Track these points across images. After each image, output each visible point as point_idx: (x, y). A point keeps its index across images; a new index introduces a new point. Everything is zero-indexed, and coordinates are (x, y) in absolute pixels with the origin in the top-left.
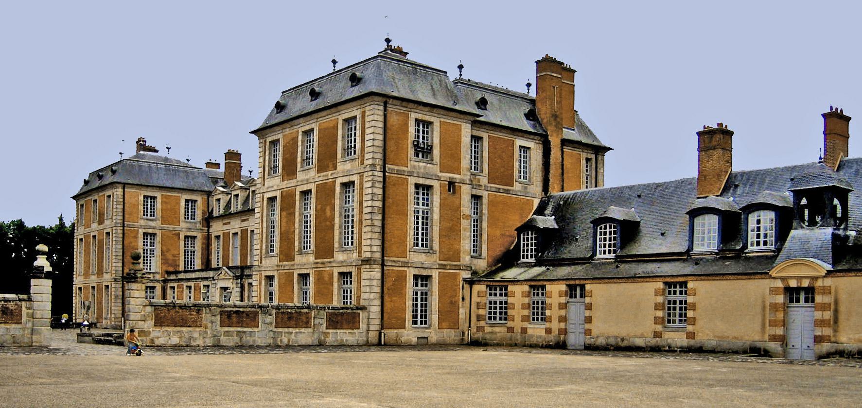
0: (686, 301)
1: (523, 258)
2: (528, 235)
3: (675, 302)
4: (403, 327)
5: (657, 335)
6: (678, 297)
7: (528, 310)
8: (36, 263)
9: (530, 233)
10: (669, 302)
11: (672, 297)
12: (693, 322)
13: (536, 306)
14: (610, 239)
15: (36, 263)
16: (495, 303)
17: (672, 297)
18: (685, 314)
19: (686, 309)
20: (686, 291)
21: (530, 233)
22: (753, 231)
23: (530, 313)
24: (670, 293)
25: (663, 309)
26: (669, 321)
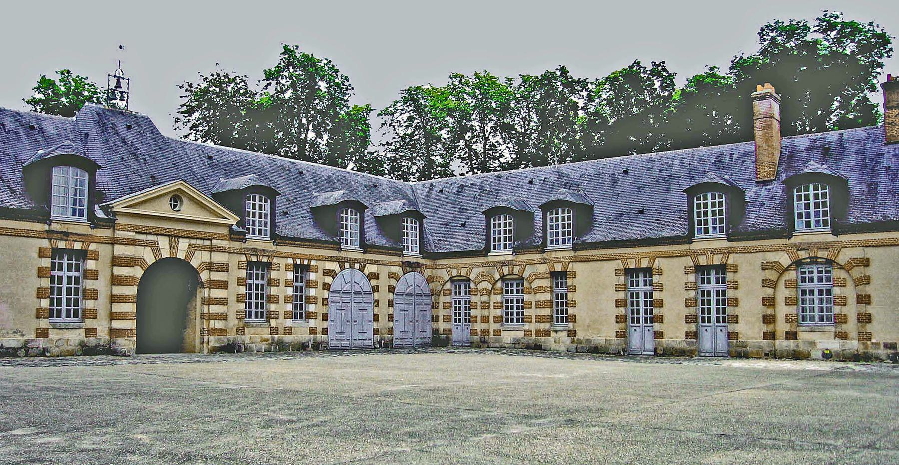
0: (523, 300)
1: (495, 248)
2: (500, 220)
3: (512, 301)
4: (766, 337)
5: (43, 333)
6: (515, 296)
7: (795, 306)
8: (849, 54)
9: (560, 211)
10: (507, 301)
11: (510, 296)
12: (660, 319)
13: (510, 304)
14: (505, 231)
15: (849, 54)
16: (811, 292)
17: (510, 296)
18: (523, 313)
19: (523, 308)
20: (522, 290)
21: (560, 211)
22: (800, 216)
23: (797, 309)
24: (507, 292)
25: (625, 305)
26: (507, 320)
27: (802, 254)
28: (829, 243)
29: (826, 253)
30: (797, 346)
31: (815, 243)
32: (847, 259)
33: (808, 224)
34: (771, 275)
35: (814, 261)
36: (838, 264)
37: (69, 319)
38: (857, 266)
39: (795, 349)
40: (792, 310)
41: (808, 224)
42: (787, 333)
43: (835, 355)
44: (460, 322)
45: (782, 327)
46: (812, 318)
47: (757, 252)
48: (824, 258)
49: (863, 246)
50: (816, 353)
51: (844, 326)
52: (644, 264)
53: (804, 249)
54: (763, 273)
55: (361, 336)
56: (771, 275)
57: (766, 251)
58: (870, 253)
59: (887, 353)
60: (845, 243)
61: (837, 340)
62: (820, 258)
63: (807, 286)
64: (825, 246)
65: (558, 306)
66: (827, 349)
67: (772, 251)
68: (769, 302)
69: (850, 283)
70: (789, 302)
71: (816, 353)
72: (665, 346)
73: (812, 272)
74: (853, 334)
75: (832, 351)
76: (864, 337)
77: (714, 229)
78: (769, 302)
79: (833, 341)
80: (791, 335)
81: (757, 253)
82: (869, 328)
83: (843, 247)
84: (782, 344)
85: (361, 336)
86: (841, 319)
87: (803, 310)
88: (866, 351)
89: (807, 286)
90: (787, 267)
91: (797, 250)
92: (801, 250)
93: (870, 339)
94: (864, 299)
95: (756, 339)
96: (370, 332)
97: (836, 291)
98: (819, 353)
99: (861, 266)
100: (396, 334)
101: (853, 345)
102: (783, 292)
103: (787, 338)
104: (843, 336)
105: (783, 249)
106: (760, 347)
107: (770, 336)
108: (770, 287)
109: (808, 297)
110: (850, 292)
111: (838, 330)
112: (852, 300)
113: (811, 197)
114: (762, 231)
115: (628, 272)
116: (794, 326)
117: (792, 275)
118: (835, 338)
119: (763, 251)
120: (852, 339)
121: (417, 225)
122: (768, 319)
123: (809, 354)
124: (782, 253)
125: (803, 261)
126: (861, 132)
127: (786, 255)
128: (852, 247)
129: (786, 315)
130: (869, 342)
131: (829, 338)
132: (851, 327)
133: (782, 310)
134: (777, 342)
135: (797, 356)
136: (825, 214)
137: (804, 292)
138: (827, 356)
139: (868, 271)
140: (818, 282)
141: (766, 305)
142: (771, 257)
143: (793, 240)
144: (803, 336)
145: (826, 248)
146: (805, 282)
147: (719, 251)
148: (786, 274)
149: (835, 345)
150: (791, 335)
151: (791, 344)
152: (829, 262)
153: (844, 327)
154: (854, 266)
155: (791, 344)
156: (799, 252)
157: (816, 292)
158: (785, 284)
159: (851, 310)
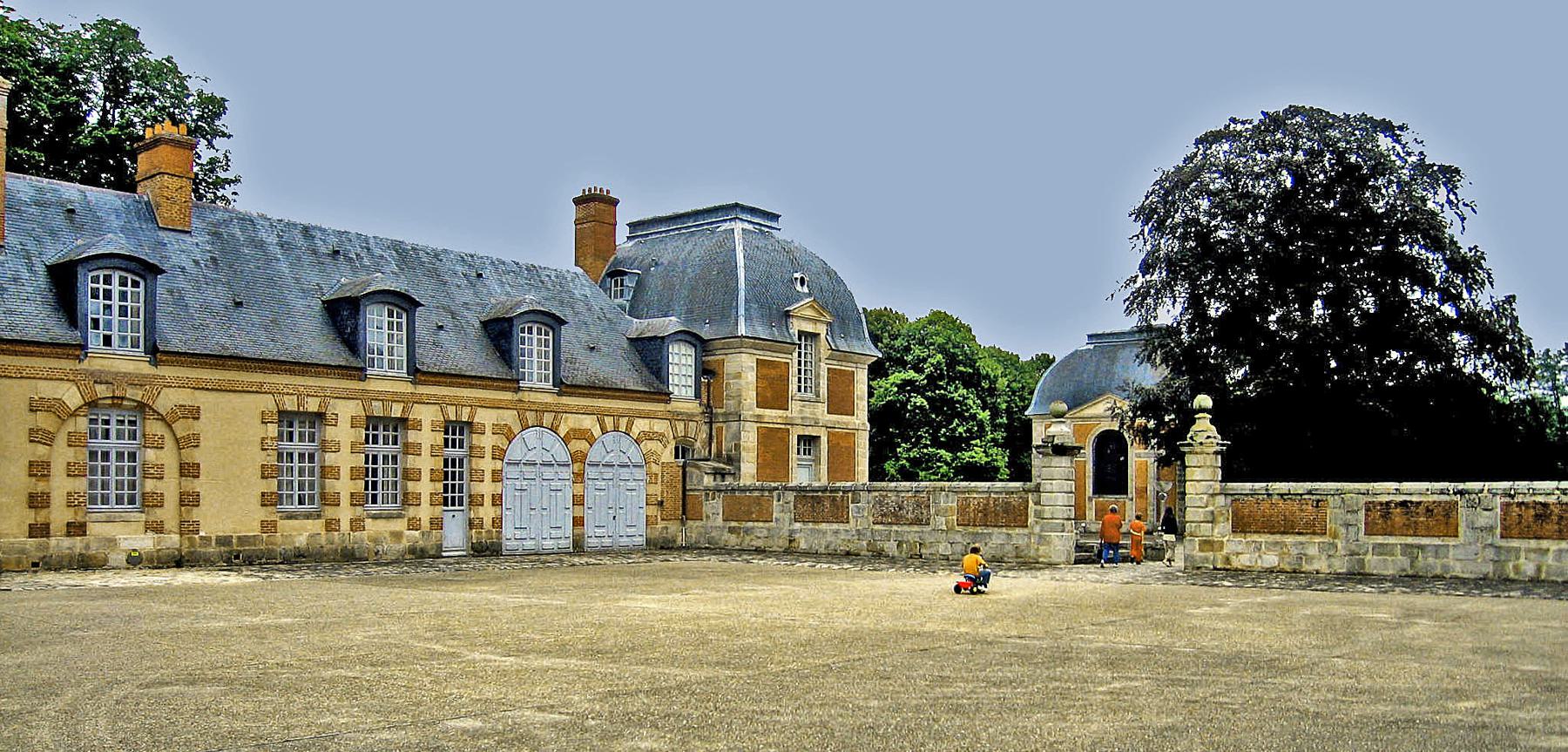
23: (142, 485)
27: (102, 390)
28: (145, 376)
29: (141, 393)
30: (87, 547)
31: (125, 373)
32: (170, 405)
33: (107, 341)
34: (44, 421)
35: (117, 402)
36: (155, 411)
37: (120, 506)
38: (183, 417)
39: (84, 552)
40: (81, 485)
41: (107, 341)
42: (69, 525)
43: (147, 559)
44: (461, 504)
45: (59, 515)
46: (105, 500)
47: (21, 377)
48: (134, 400)
49: (193, 388)
50: (118, 558)
51: (158, 511)
52: (312, 405)
53: (107, 383)
54: (31, 416)
55: (519, 534)
56: (44, 421)
57: (40, 378)
58: (203, 400)
59: (220, 552)
60: (169, 380)
61: (150, 534)
62: (129, 399)
63: (99, 444)
64: (138, 381)
65: (461, 474)
66: (135, 550)
67: (51, 379)
68: (39, 469)
69: (169, 443)
70: (72, 471)
71: (118, 558)
72: (297, 545)
73: (107, 422)
74: (171, 523)
75: (142, 552)
76: (187, 528)
77: (124, 339)
78: (39, 469)
79: (142, 536)
80: (75, 529)
81: (23, 380)
82: (196, 514)
83: (165, 386)
84: (60, 544)
85: (519, 534)
86: (151, 502)
87: (133, 486)
88: (193, 549)
89: (99, 444)
90: (75, 411)
91: (95, 382)
92: (101, 383)
93: (197, 532)
94: (189, 470)
95: (15, 537)
96: (641, 526)
97: (151, 455)
98: (124, 557)
99: (189, 418)
100: (508, 531)
101: (173, 540)
102: (62, 455)
103: (68, 534)
104: (157, 528)
105: (71, 378)
106: (23, 551)
107: (40, 530)
108: (44, 444)
109: (100, 463)
110: (167, 458)
111: (152, 518)
112: (172, 470)
113: (116, 296)
114: (583, 386)
115: (285, 417)
116: (80, 514)
117: (82, 424)
118: (146, 531)
119: (34, 378)
120: (170, 532)
121: (551, 337)
122: (38, 501)
123: (106, 560)
124: (68, 385)
125: (100, 402)
126: (113, 198)
127: (75, 388)
128: (179, 387)
129: (69, 494)
130: (197, 536)
131: (136, 532)
132: (168, 513)
133: (60, 486)
134: (53, 541)
135: (86, 564)
136: (135, 329)
137: (93, 455)
138: (134, 561)
139: (198, 427)
140: (117, 439)
141: (36, 475)
142: (47, 390)
143: (85, 365)
144: (94, 529)
145: (141, 385)
146: (97, 438)
147: (397, 398)
148: (71, 422)
149: (145, 543)
150: (75, 529)
151: (77, 543)
152: (142, 407)
153: (159, 514)
154: (180, 418)
155: (77, 543)
156: (98, 388)
157: (113, 456)
158: (69, 440)
159: (170, 487)
